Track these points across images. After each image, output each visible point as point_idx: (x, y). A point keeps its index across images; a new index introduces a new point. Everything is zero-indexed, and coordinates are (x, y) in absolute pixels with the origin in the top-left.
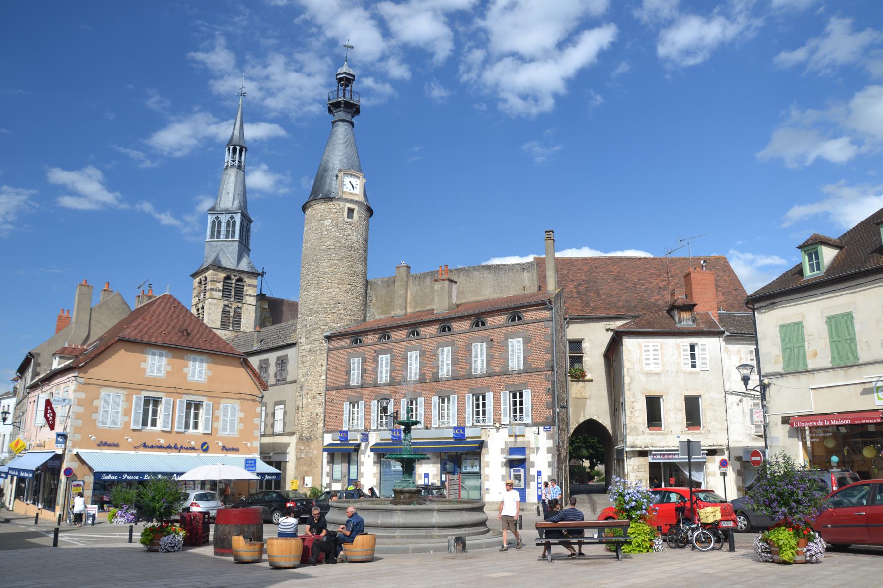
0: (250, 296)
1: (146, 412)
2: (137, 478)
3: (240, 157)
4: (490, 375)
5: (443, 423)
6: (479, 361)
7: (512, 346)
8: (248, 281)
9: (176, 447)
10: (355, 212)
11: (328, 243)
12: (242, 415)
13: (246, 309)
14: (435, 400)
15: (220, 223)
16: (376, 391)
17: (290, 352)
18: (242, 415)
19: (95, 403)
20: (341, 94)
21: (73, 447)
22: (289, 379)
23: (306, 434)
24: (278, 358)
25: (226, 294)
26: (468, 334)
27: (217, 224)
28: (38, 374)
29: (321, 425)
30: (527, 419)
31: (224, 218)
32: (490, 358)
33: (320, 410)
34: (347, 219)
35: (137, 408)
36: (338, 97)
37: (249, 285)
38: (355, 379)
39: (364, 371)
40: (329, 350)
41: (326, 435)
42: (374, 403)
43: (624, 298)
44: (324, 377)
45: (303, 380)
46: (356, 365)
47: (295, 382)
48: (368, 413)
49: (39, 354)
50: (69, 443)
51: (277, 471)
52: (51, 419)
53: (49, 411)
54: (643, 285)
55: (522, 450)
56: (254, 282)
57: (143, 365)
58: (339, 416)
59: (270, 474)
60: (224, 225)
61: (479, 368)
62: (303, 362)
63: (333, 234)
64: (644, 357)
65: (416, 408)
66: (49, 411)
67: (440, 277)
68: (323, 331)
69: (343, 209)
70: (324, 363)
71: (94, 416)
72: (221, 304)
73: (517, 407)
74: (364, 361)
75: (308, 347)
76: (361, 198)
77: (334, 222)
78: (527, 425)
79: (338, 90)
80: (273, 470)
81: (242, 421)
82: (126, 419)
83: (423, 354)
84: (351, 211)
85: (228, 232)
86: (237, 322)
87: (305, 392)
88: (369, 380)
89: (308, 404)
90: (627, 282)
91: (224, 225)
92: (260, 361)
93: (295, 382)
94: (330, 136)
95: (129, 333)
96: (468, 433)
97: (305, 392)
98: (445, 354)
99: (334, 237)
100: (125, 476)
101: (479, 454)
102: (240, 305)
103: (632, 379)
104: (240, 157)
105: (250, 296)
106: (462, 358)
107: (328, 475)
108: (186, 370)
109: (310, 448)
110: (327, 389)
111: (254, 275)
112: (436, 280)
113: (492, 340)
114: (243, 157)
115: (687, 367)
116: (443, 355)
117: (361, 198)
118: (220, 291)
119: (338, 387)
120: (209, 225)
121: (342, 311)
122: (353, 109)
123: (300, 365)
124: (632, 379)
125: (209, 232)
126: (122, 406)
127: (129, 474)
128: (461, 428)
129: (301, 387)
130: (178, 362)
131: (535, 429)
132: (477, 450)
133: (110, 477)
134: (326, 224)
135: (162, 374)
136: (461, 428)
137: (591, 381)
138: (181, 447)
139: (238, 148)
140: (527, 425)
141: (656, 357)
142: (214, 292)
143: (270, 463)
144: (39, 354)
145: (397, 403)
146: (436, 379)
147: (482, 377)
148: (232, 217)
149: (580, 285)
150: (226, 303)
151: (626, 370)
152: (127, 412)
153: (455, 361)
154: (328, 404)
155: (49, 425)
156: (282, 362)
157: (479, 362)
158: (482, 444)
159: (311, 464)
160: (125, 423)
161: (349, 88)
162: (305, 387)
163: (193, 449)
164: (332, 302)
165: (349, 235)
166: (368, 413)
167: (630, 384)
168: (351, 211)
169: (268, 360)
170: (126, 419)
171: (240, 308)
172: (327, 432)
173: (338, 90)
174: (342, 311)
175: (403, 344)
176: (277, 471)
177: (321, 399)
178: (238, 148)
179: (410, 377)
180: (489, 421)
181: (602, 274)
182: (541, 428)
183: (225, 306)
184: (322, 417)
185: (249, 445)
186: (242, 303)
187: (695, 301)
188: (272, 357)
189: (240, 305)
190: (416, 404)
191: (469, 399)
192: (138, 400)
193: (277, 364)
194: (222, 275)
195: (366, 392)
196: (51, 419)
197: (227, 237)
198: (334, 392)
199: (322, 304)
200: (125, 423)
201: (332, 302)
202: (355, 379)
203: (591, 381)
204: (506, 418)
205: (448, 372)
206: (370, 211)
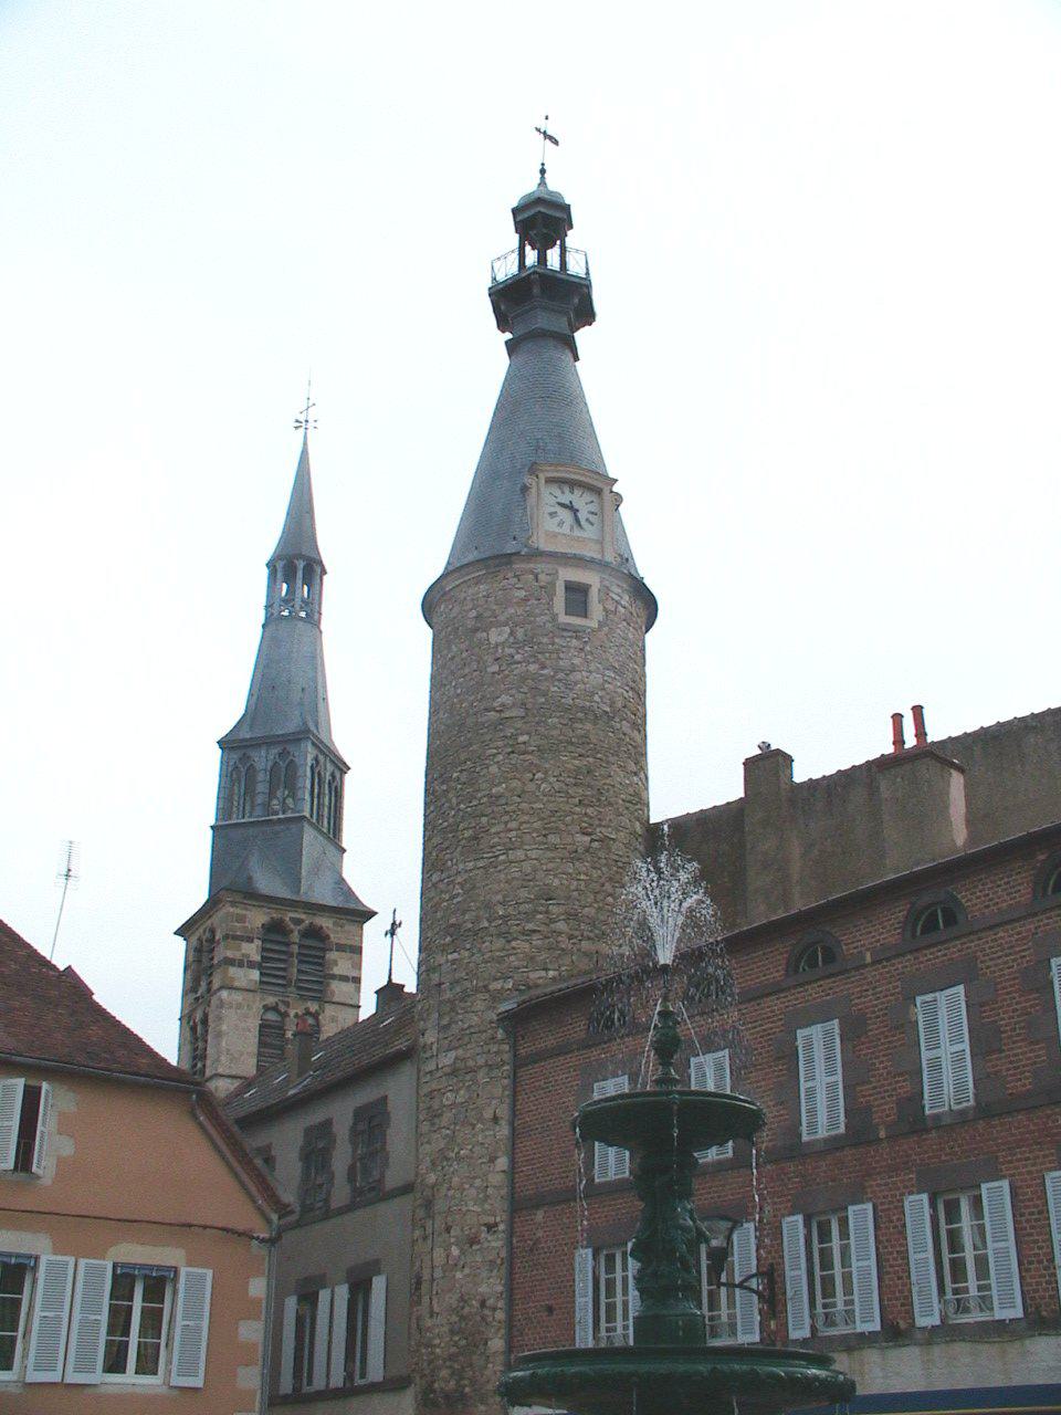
5: (962, 1307)
11: (505, 699)
14: (917, 1206)
17: (398, 1090)
22: (393, 1179)
23: (445, 1381)
25: (272, 974)
26: (1030, 925)
29: (497, 1344)
33: (491, 1286)
40: (518, 1064)
44: (502, 1162)
45: (432, 1178)
47: (407, 1189)
61: (948, 1088)
62: (435, 1115)
63: (519, 669)
65: (845, 1250)
68: (496, 997)
69: (549, 589)
70: (504, 1111)
75: (447, 1059)
77: (520, 633)
83: (853, 1032)
87: (439, 1223)
89: (451, 1266)
92: (308, 1132)
97: (439, 1223)
98: (943, 1014)
99: (523, 679)
102: (314, 1007)
110: (519, 1205)
115: (56, 1272)
118: (252, 965)
123: (425, 1127)
129: (428, 1204)
142: (232, 971)
145: (771, 1235)
146: (912, 1119)
150: (271, 1000)
156: (372, 1122)
157: (947, 1066)
162: (440, 1205)
164: (523, 894)
165: (573, 669)
169: (328, 1123)
174: (561, 926)
175: (774, 1004)
177: (496, 1243)
179: (812, 1126)
183: (267, 1008)
184: (500, 1315)
188: (341, 1112)
189: (314, 1007)
190: (844, 1234)
193: (355, 1133)
194: (258, 918)
198: (540, 1216)
199: (488, 906)
201: (523, 894)
205: (960, 1087)
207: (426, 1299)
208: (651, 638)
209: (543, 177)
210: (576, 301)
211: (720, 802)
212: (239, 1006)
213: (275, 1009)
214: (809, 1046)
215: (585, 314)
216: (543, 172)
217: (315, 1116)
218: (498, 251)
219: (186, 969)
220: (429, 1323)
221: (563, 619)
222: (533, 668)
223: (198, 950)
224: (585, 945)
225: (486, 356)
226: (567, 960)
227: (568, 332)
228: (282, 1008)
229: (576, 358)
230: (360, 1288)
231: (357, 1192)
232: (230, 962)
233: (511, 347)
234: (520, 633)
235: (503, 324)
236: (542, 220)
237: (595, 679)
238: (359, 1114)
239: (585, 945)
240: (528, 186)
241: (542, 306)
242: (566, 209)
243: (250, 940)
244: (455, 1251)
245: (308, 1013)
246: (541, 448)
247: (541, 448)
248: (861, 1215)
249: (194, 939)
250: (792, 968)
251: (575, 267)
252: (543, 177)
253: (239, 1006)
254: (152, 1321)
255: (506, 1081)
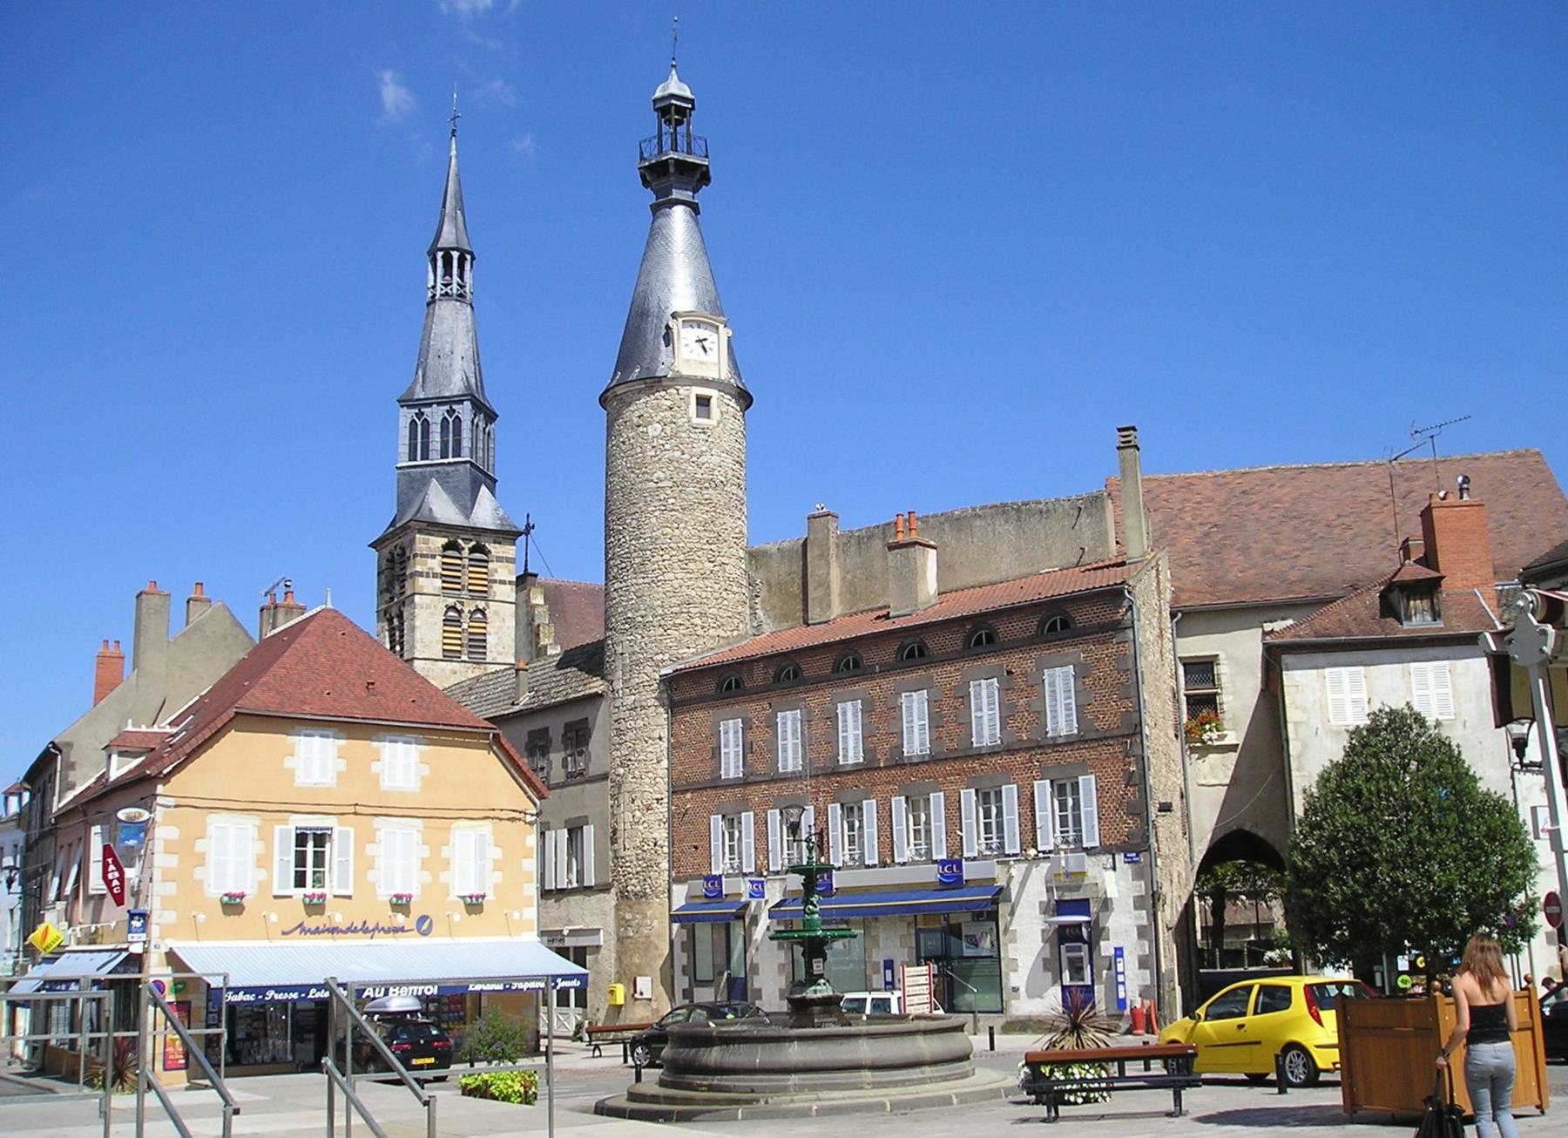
0: (503, 582)
1: (301, 859)
2: (295, 996)
3: (461, 276)
4: (1010, 751)
6: (986, 720)
7: (1052, 684)
8: (495, 549)
9: (365, 930)
10: (713, 402)
12: (497, 853)
13: (496, 613)
15: (426, 423)
16: (775, 790)
18: (497, 853)
19: (200, 846)
20: (667, 140)
21: (162, 938)
22: (594, 770)
24: (568, 727)
27: (420, 431)
28: (72, 787)
29: (665, 865)
30: (1092, 839)
31: (435, 414)
32: (1008, 714)
33: (661, 834)
34: (696, 421)
35: (283, 852)
36: (661, 152)
37: (500, 559)
38: (732, 767)
39: (748, 748)
41: (675, 887)
42: (774, 816)
43: (1303, 561)
44: (665, 763)
46: (731, 733)
47: (605, 777)
48: (762, 835)
49: (70, 745)
50: (155, 930)
51: (579, 970)
52: (116, 883)
53: (112, 867)
54: (1349, 527)
55: (1082, 906)
56: (508, 550)
57: (289, 763)
58: (702, 847)
59: (566, 977)
60: (435, 430)
63: (668, 454)
64: (1331, 696)
66: (112, 867)
67: (901, 538)
70: (665, 733)
71: (198, 873)
72: (442, 603)
73: (1070, 820)
74: (747, 726)
76: (725, 373)
78: (1089, 851)
79: (660, 137)
80: (572, 968)
81: (498, 866)
82: (262, 875)
83: (868, 710)
84: (703, 402)
85: (444, 444)
86: (478, 645)
88: (760, 767)
90: (1313, 522)
91: (435, 430)
93: (605, 777)
94: (655, 234)
95: (257, 699)
96: (969, 871)
98: (915, 706)
100: (271, 993)
101: (994, 916)
103: (1305, 746)
104: (461, 276)
105: (503, 582)
106: (949, 714)
107: (685, 971)
108: (376, 767)
109: (645, 916)
110: (676, 790)
111: (507, 535)
112: (891, 548)
113: (1009, 673)
114: (467, 274)
116: (909, 708)
117: (725, 373)
118: (435, 575)
119: (694, 785)
120: (405, 432)
121: (697, 621)
122: (697, 176)
124: (1305, 746)
125: (404, 450)
126: (254, 847)
127: (279, 989)
128: (953, 863)
130: (359, 746)
131: (1106, 859)
132: (990, 908)
133: (241, 997)
134: (651, 432)
135: (330, 780)
136: (953, 863)
137: (1426, 515)
138: (376, 929)
139: (455, 254)
140: (1089, 851)
141: (1356, 696)
143: (563, 952)
144: (70, 745)
145: (821, 813)
147: (993, 753)
148: (451, 412)
149: (1207, 535)
150: (451, 601)
151: (1290, 727)
152: (263, 861)
153: (936, 721)
154: (676, 820)
155: (114, 895)
158: (1001, 894)
159: (647, 949)
160: (260, 883)
161: (681, 129)
163: (402, 930)
166: (762, 835)
167: (1299, 756)
168: (703, 402)
170: (262, 875)
171: (483, 612)
172: (678, 880)
173: (660, 137)
176: (579, 970)
178: (455, 254)
180: (1012, 847)
181: (1256, 507)
182: (1120, 858)
183: (449, 608)
185: (516, 915)
186: (485, 599)
187: (1443, 573)
189: (481, 605)
191: (969, 797)
192: (284, 833)
195: (756, 794)
196: (116, 883)
197: (444, 455)
200: (260, 883)
202: (732, 767)
203: (1426, 515)
204: (1049, 837)
206: (745, 398)
207: (620, 841)
212: (428, 607)
213: (453, 608)
214: (844, 714)
217: (538, 724)
219: (379, 574)
220: (622, 853)
221: (696, 421)
222: (678, 454)
223: (391, 560)
224: (712, 632)
226: (701, 642)
228: (459, 607)
230: (575, 831)
231: (570, 775)
232: (421, 574)
234: (668, 429)
237: (715, 459)
238: (568, 727)
239: (712, 632)
243: (434, 557)
244: (638, 814)
245: (478, 610)
248: (748, 818)
249: (386, 551)
250: (836, 669)
253: (428, 607)
254: (319, 859)
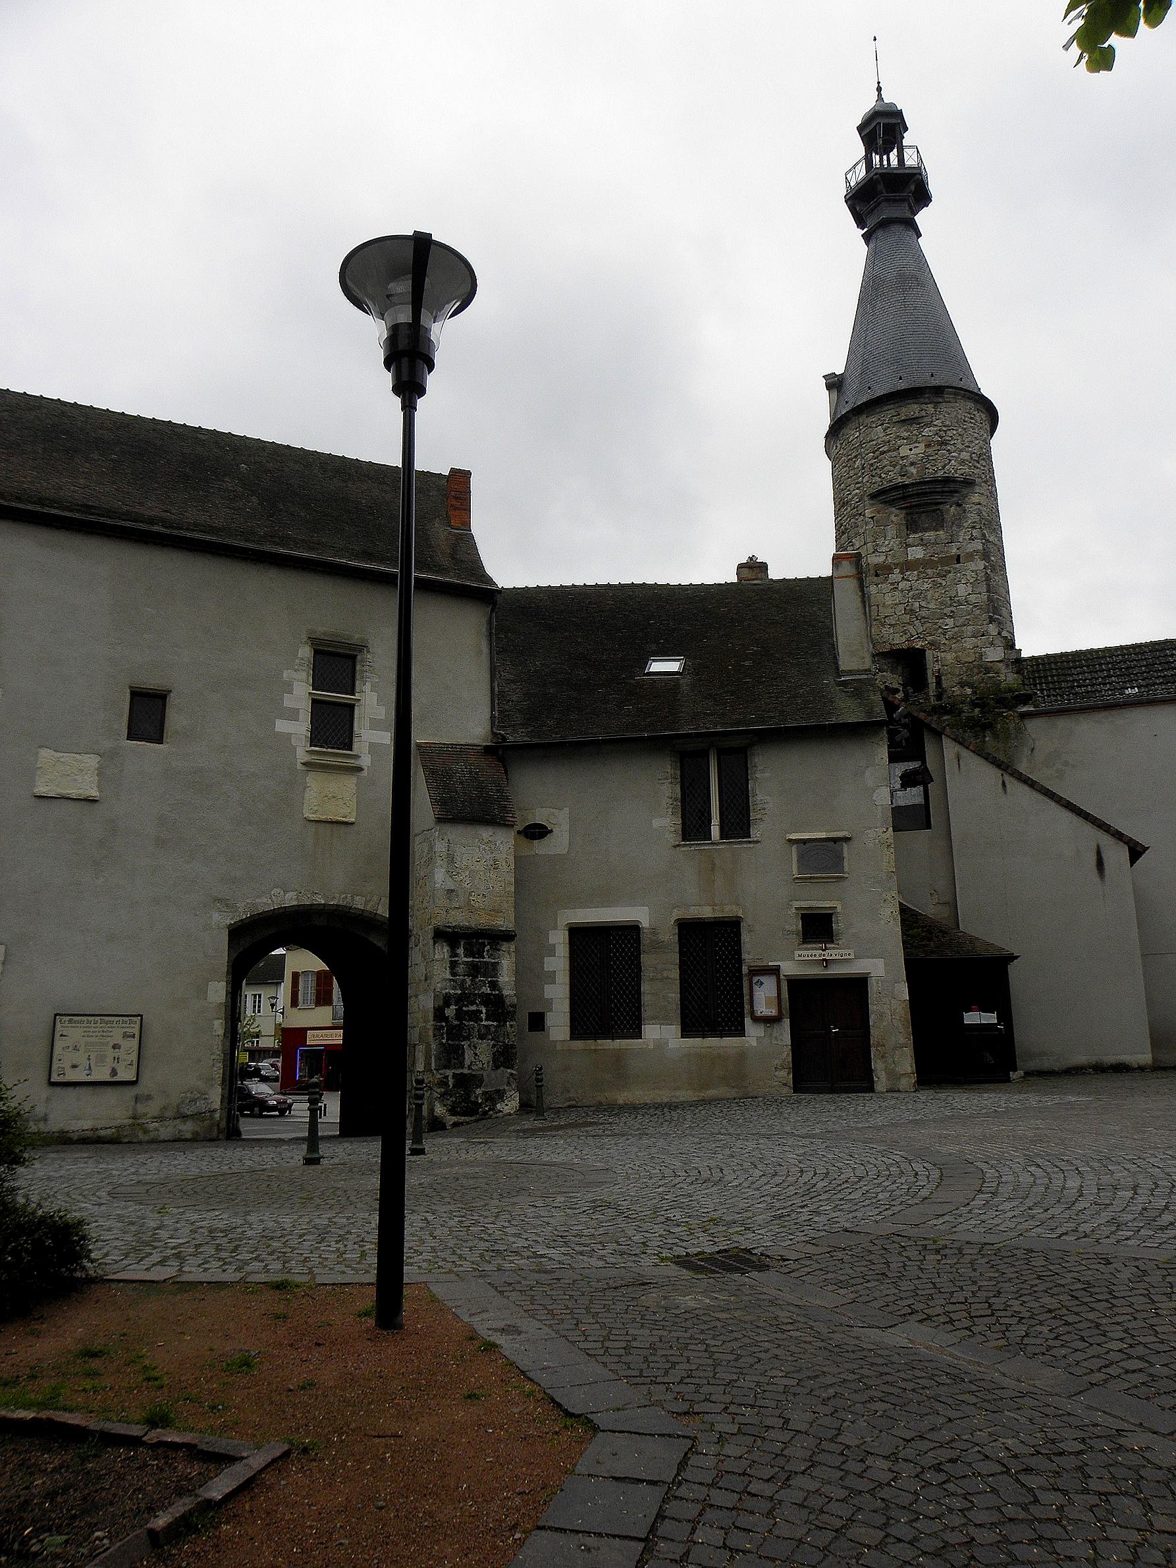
208: (995, 442)
209: (879, 95)
210: (913, 188)
211: (364, 457)
215: (922, 197)
216: (879, 89)
218: (848, 157)
225: (847, 249)
227: (908, 215)
229: (919, 235)
233: (867, 238)
235: (860, 222)
236: (882, 129)
240: (868, 103)
241: (888, 197)
242: (899, 114)
246: (899, 299)
247: (899, 299)
251: (910, 160)
252: (879, 95)
255: (783, 1073)
